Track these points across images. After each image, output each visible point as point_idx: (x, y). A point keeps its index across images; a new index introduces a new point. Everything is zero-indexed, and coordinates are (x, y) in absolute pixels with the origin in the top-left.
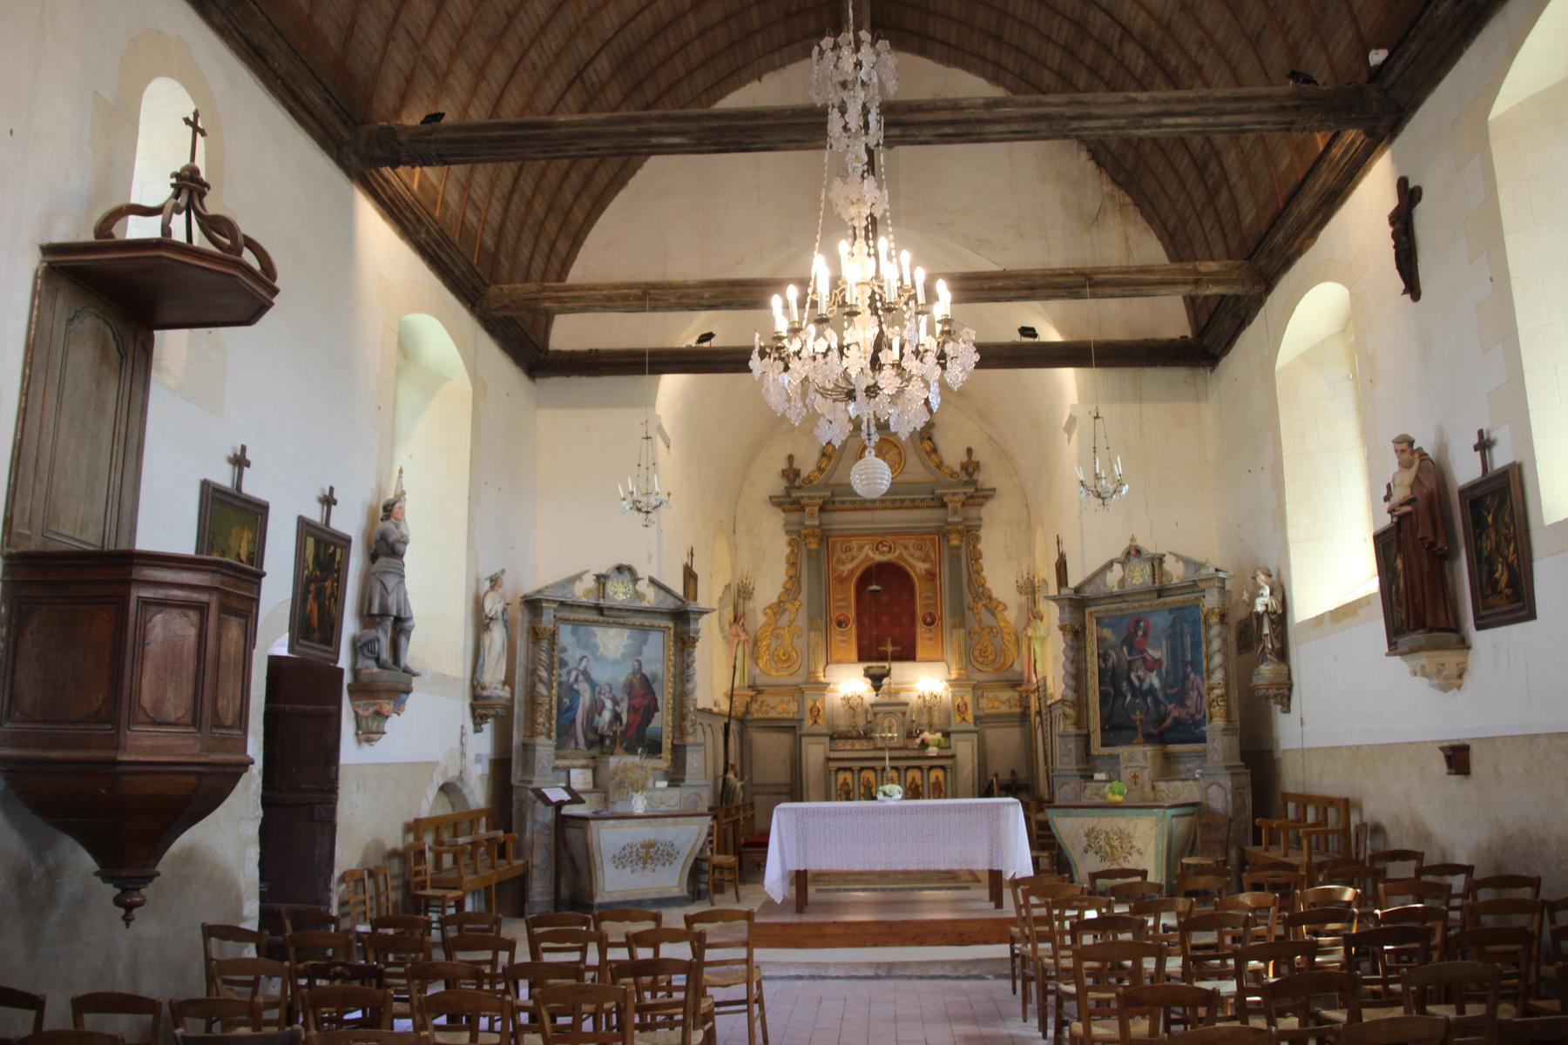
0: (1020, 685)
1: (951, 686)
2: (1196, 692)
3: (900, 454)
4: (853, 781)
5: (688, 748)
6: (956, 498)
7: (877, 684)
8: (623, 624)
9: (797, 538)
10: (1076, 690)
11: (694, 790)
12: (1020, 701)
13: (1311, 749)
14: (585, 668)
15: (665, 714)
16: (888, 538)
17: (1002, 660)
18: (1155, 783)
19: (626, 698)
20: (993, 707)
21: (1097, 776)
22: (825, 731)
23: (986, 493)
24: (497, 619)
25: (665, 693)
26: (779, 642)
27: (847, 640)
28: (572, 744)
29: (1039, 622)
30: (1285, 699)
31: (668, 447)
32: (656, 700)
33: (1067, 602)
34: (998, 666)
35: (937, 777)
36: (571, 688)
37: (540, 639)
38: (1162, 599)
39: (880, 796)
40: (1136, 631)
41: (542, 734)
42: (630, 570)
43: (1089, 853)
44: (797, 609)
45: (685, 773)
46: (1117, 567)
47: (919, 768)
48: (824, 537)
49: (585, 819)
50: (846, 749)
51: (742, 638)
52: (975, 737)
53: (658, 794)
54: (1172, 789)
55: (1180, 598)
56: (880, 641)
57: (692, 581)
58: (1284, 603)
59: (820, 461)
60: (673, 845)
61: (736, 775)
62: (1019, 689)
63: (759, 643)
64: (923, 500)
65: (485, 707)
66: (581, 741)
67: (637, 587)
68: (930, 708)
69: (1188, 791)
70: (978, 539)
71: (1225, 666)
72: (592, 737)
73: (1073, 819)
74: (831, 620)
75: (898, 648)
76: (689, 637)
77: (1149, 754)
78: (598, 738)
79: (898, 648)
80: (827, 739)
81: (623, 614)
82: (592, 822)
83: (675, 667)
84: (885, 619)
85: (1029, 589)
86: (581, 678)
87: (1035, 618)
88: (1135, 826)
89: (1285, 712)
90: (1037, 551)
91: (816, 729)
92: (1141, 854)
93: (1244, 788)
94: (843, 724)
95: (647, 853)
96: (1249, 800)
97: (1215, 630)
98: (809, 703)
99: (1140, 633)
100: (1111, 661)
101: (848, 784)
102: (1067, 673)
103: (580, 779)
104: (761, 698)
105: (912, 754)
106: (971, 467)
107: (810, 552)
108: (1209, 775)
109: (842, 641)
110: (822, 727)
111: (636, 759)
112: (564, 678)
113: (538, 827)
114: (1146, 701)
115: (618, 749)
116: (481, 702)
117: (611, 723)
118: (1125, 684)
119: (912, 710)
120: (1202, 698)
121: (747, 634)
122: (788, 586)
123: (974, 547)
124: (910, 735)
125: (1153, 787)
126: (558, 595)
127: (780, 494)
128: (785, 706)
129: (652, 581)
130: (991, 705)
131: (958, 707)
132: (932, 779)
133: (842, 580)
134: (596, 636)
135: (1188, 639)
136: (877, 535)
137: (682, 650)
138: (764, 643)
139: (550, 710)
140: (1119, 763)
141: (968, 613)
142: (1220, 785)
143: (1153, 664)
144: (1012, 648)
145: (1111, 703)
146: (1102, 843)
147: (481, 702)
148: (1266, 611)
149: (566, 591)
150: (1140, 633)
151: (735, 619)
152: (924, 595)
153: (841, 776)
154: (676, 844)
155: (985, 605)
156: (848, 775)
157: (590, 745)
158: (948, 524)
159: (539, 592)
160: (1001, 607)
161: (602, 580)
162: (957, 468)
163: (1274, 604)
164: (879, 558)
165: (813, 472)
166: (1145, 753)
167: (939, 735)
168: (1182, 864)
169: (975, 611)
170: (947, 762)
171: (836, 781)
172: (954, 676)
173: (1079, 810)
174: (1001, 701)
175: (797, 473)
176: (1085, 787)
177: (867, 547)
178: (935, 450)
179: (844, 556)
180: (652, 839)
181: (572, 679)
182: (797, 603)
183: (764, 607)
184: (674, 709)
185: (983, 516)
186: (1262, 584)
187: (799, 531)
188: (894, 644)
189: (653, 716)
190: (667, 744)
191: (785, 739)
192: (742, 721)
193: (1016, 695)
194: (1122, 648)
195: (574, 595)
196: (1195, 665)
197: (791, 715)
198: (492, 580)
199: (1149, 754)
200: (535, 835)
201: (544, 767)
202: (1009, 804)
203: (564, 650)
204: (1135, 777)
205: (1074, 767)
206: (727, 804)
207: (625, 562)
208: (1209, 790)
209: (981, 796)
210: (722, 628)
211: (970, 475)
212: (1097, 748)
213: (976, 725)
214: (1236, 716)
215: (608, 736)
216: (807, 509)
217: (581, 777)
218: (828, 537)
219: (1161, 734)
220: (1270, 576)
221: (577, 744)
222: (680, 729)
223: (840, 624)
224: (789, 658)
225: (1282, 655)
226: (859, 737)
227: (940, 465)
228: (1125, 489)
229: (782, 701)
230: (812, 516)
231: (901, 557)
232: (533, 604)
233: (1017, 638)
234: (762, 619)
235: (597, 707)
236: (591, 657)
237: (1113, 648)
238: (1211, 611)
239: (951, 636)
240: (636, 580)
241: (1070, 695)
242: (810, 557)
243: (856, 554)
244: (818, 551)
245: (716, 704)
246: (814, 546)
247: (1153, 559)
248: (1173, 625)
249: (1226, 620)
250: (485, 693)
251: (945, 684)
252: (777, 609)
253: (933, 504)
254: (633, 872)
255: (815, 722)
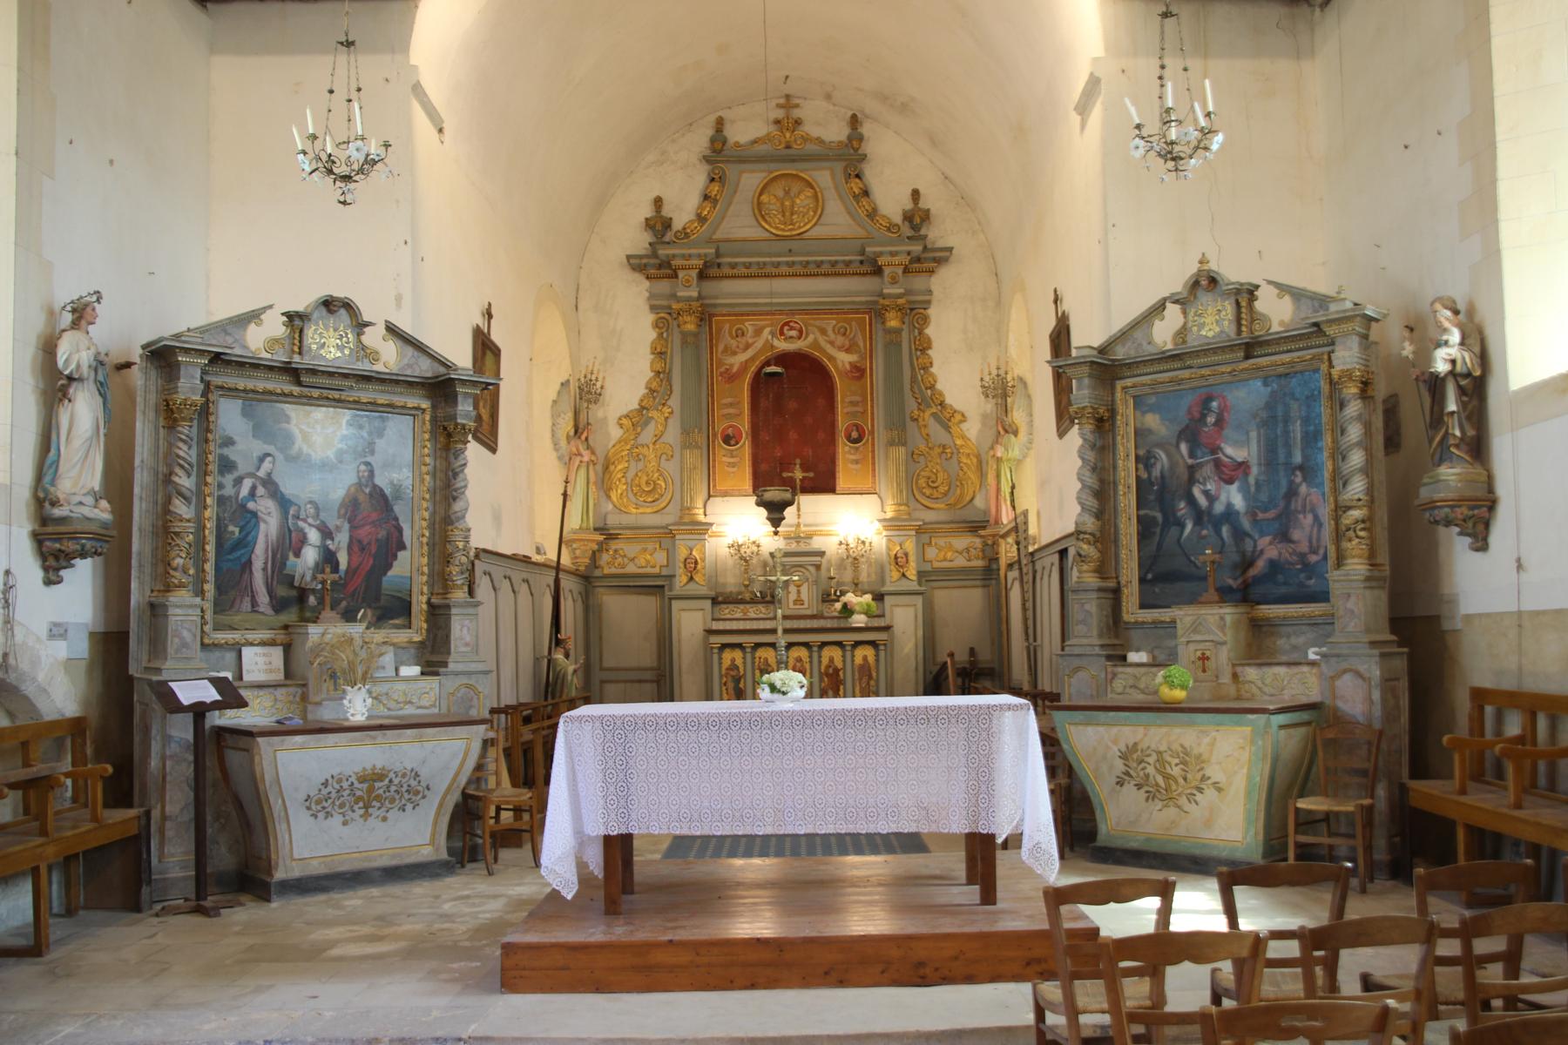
0: (984, 528)
1: (886, 528)
2: (1310, 517)
3: (816, 197)
4: (744, 663)
5: (454, 611)
6: (897, 260)
7: (777, 516)
8: (339, 401)
9: (666, 316)
10: (1099, 515)
11: (464, 680)
12: (983, 551)
13: (1538, 613)
14: (269, 474)
15: (416, 554)
16: (797, 318)
17: (958, 492)
18: (1239, 669)
19: (346, 526)
20: (945, 560)
21: (1133, 657)
22: (704, 591)
23: (938, 254)
24: (80, 380)
25: (417, 517)
26: (640, 465)
27: (738, 464)
28: (246, 604)
29: (1013, 436)
30: (1481, 527)
31: (441, 131)
32: (400, 530)
33: (1086, 369)
34: (952, 501)
35: (865, 658)
36: (243, 507)
37: (175, 420)
38: (1252, 361)
39: (765, 693)
40: (1203, 417)
41: (181, 586)
42: (348, 305)
43: (1126, 786)
44: (667, 418)
45: (449, 653)
46: (1173, 311)
47: (839, 644)
48: (706, 316)
49: (249, 734)
50: (735, 618)
51: (586, 459)
52: (919, 600)
53: (400, 686)
54: (1268, 681)
55: (1286, 357)
56: (786, 465)
57: (489, 356)
58: (1483, 358)
59: (700, 207)
60: (417, 775)
61: (567, 656)
62: (982, 532)
63: (612, 468)
64: (848, 264)
65: (58, 537)
66: (263, 598)
67: (364, 338)
68: (855, 559)
69: (1303, 685)
70: (925, 320)
71: (1367, 470)
72: (282, 591)
73: (1101, 729)
74: (715, 435)
75: (811, 475)
76: (457, 425)
77: (1228, 619)
78: (294, 593)
79: (811, 475)
80: (709, 602)
81: (337, 382)
82: (260, 740)
83: (434, 476)
84: (793, 435)
85: (1001, 391)
86: (261, 491)
87: (1006, 431)
88: (1212, 744)
89: (1477, 550)
90: (1011, 337)
91: (692, 589)
92: (1219, 790)
93: (1397, 679)
94: (731, 582)
95: (371, 790)
96: (1405, 702)
97: (1354, 408)
98: (682, 553)
99: (1211, 419)
100: (1159, 466)
101: (737, 668)
102: (1084, 486)
103: (260, 663)
104: (614, 545)
105: (829, 624)
106: (917, 218)
107: (684, 335)
108: (1338, 656)
109: (733, 465)
110: (701, 586)
111: (356, 630)
112: (229, 491)
113: (173, 748)
114: (1218, 532)
115: (327, 614)
116: (50, 529)
117: (318, 568)
118: (1182, 505)
119: (829, 562)
120: (1320, 525)
121: (593, 453)
122: (654, 385)
123: (920, 333)
124: (827, 598)
125: (1235, 676)
126: (216, 344)
127: (643, 252)
128: (648, 557)
129: (392, 330)
130: (941, 556)
131: (896, 557)
132: (858, 660)
133: (731, 377)
134: (288, 419)
135: (1297, 429)
136: (781, 313)
137: (447, 448)
138: (620, 467)
139: (200, 542)
140: (1175, 636)
141: (911, 425)
142: (1358, 674)
143: (1232, 472)
144: (973, 476)
145: (1157, 538)
146: (1151, 770)
147: (50, 529)
148: (1452, 373)
149: (229, 340)
150: (1211, 419)
151: (576, 432)
152: (847, 400)
153: (728, 656)
154: (424, 773)
155: (934, 415)
156: (738, 654)
157: (279, 605)
158: (883, 296)
159: (177, 337)
160: (958, 417)
161: (297, 322)
162: (898, 219)
163: (1466, 360)
164: (782, 345)
165: (691, 222)
166: (1222, 619)
167: (868, 597)
168: (1297, 810)
169: (921, 423)
170: (879, 636)
171: (720, 663)
172: (889, 515)
173: (1112, 714)
174: (957, 550)
175: (667, 224)
176: (1114, 675)
177: (767, 331)
178: (866, 193)
179: (733, 343)
180: (379, 766)
181: (245, 491)
182: (667, 410)
183: (618, 415)
184: (432, 545)
185: (933, 288)
186: (1447, 324)
187: (670, 308)
188: (805, 468)
189: (395, 557)
190: (419, 604)
191: (649, 603)
192: (587, 579)
193: (978, 542)
194: (1178, 446)
195: (245, 347)
196: (1308, 470)
197: (657, 570)
198: (74, 311)
199: (1228, 619)
200: (168, 763)
201: (185, 645)
202: (1001, 707)
203: (229, 442)
204: (1204, 658)
205: (1097, 641)
206: (553, 698)
207: (339, 293)
208: (1338, 683)
209: (928, 691)
210: (556, 445)
211: (916, 228)
212: (1131, 610)
213: (920, 584)
214: (1384, 557)
215: (314, 591)
216: (681, 274)
217: (261, 660)
218: (711, 316)
219: (1246, 586)
220: (1456, 312)
221: (254, 604)
222: (440, 580)
223: (727, 440)
224: (654, 489)
225: (1478, 448)
226: (753, 601)
227: (873, 214)
228: (1217, 141)
229: (645, 550)
230: (687, 285)
231: (816, 345)
232: (162, 356)
233: (980, 462)
234: (616, 433)
235: (291, 542)
236: (280, 457)
237: (1160, 445)
238: (1348, 374)
239: (887, 457)
240: (360, 326)
241: (1090, 524)
242: (684, 343)
243: (750, 341)
244: (696, 335)
245: (538, 551)
246: (691, 327)
247: (1238, 292)
248: (1270, 406)
249: (1370, 393)
250: (57, 512)
251: (879, 526)
252: (638, 419)
253: (864, 269)
254: (345, 823)
255: (691, 579)
